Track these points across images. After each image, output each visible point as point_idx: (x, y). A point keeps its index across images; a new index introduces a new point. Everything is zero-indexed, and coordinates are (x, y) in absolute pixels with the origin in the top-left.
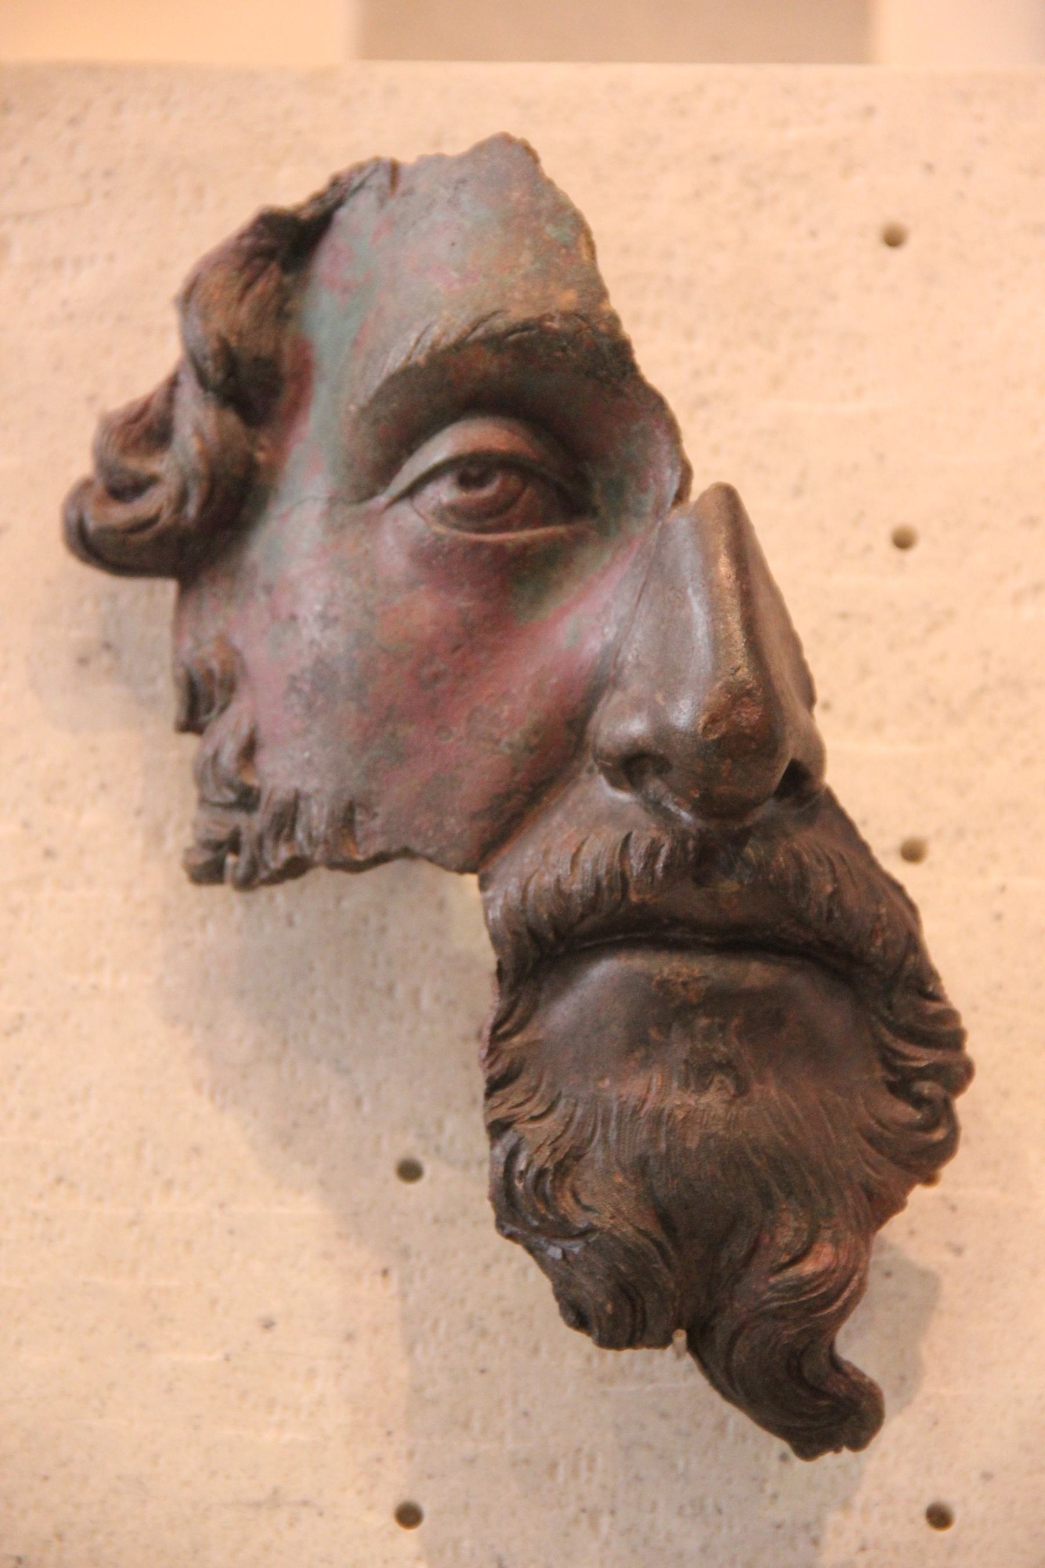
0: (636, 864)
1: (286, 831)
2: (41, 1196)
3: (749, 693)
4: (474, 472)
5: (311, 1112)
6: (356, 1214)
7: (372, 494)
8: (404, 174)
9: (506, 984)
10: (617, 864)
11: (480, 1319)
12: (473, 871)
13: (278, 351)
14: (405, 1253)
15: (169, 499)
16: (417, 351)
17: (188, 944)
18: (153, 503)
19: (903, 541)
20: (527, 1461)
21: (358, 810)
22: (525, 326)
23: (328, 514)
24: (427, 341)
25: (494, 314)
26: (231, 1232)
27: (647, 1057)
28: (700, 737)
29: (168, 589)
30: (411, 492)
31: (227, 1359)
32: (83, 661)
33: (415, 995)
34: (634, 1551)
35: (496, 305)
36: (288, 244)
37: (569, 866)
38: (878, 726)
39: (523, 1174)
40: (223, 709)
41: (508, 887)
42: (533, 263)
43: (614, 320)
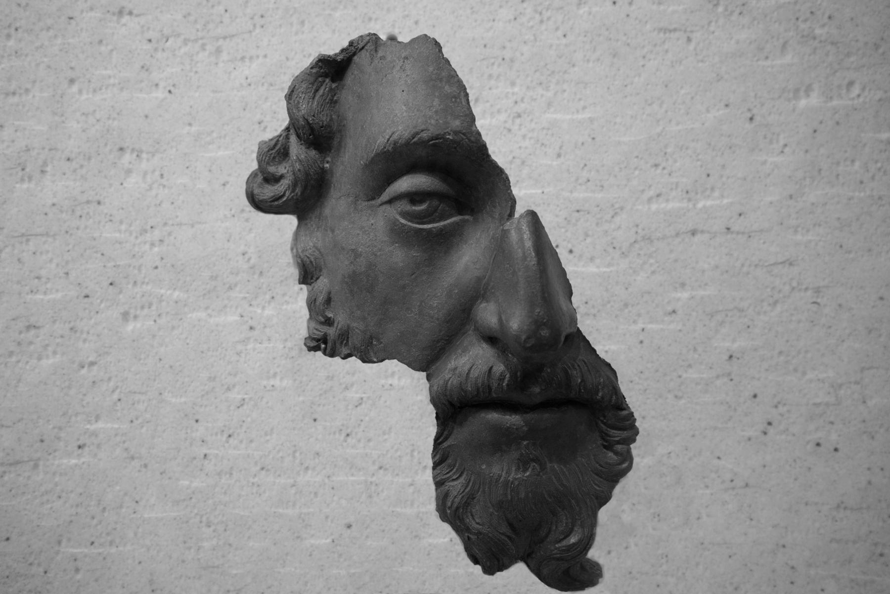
3: (544, 324)
10: (486, 382)
13: (331, 120)
22: (437, 138)
30: (390, 202)
36: (333, 70)
38: (592, 259)
43: (479, 134)
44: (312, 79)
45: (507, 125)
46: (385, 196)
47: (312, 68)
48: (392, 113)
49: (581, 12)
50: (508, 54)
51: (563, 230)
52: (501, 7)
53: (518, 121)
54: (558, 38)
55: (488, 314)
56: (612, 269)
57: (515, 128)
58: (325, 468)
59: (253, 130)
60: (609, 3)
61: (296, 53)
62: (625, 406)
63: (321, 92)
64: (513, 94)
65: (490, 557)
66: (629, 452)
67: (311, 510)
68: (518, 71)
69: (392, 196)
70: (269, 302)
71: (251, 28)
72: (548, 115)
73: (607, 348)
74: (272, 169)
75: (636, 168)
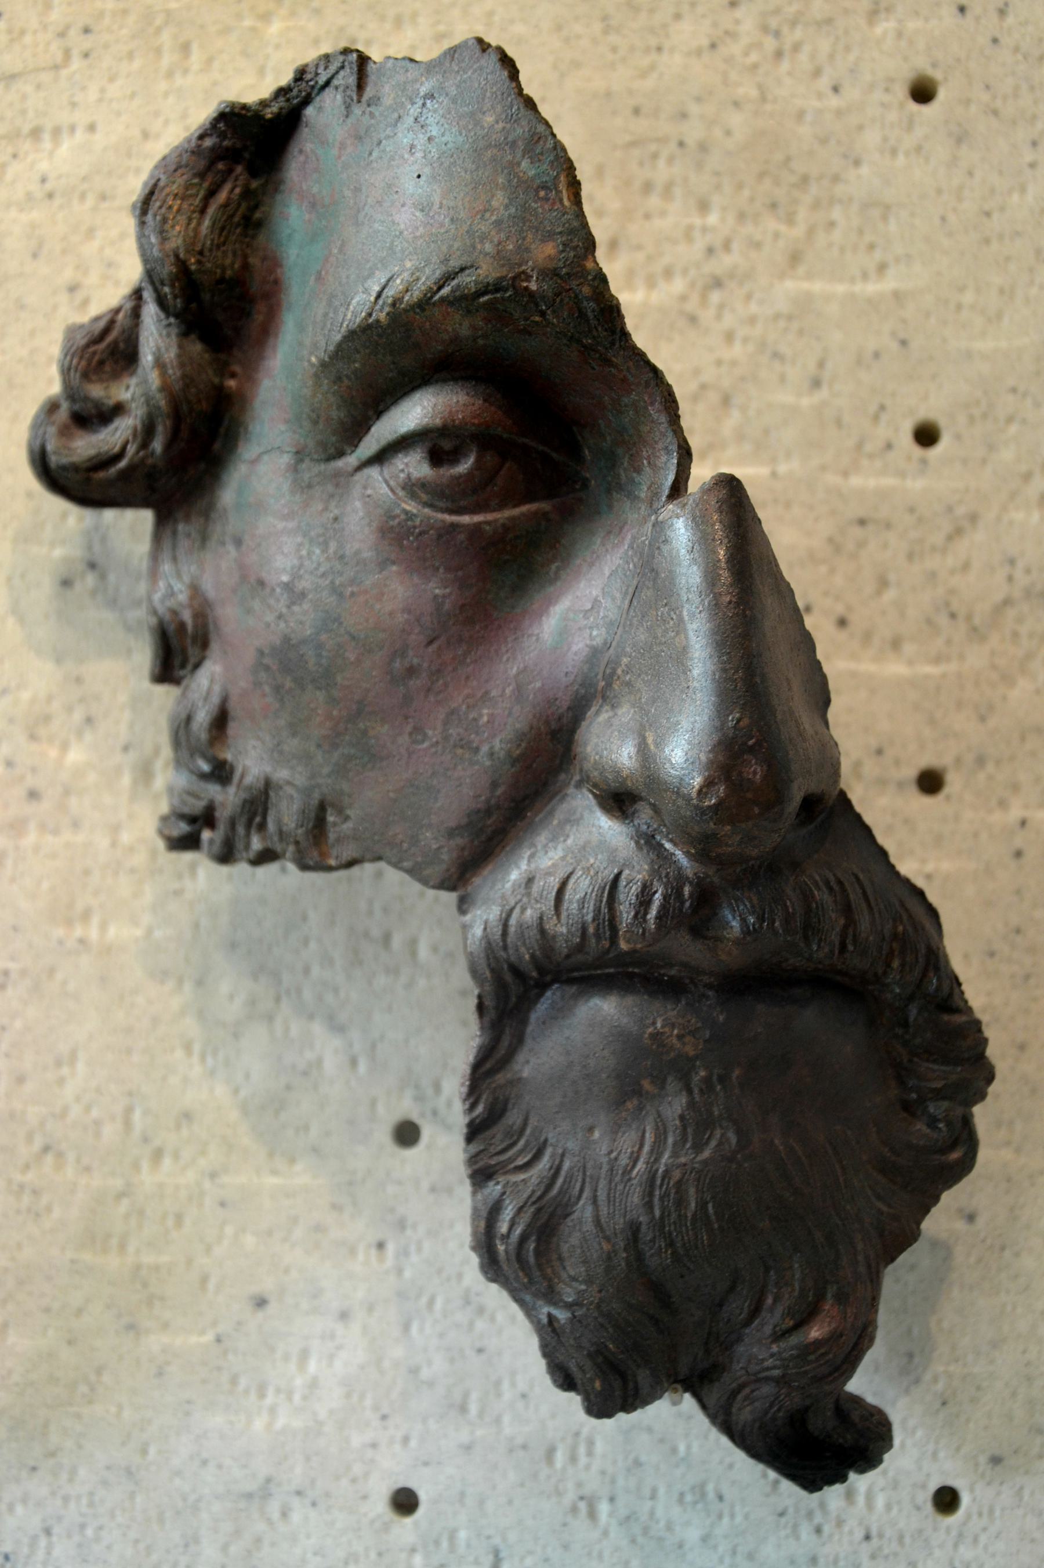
0: (626, 914)
1: (258, 819)
2: (27, 1167)
3: (751, 750)
4: (447, 445)
5: (305, 1074)
6: (351, 1183)
7: (340, 454)
8: (371, 68)
9: (487, 1019)
10: (605, 910)
11: (477, 1294)
12: (453, 888)
14: (401, 1225)
15: (135, 434)
16: (378, 307)
17: (178, 893)
18: (117, 435)
19: (926, 436)
20: (524, 1447)
21: (329, 811)
22: (497, 287)
23: (295, 468)
24: (390, 293)
25: (462, 269)
26: (223, 1204)
27: (640, 1108)
28: (695, 801)
29: (144, 518)
30: (381, 457)
31: (218, 1340)
32: (66, 583)
33: (412, 945)
34: (633, 1541)
35: (464, 260)
36: (250, 150)
37: (552, 903)
38: (896, 644)
39: (506, 1237)
40: (197, 666)
41: (484, 917)
42: (506, 207)
44: (202, 164)
45: (691, 306)
46: (370, 445)
47: (201, 137)
48: (382, 227)
49: (878, 30)
50: (693, 132)
51: (823, 569)
52: (678, 17)
53: (715, 297)
54: (820, 96)
55: (611, 744)
56: (952, 667)
57: (707, 316)
58: (203, 1153)
59: (55, 307)
60: (948, 12)
61: (166, 122)
62: (962, 1004)
63: (222, 196)
64: (704, 229)
65: (607, 1371)
66: (967, 1122)
67: (165, 1259)
68: (717, 174)
69: (383, 442)
70: (80, 734)
71: (59, 57)
72: (790, 285)
73: (929, 867)
74: (96, 391)
75: (1010, 420)
